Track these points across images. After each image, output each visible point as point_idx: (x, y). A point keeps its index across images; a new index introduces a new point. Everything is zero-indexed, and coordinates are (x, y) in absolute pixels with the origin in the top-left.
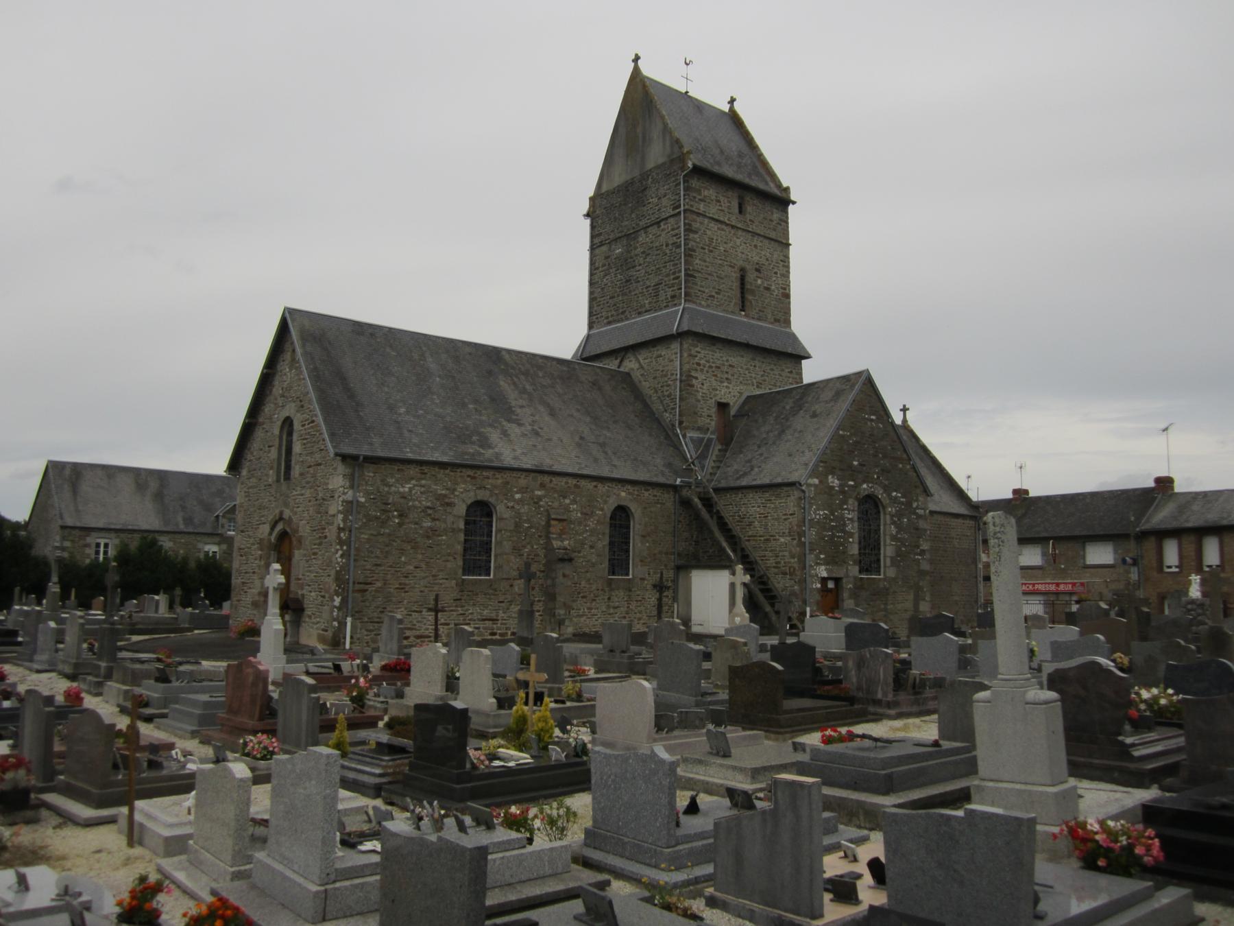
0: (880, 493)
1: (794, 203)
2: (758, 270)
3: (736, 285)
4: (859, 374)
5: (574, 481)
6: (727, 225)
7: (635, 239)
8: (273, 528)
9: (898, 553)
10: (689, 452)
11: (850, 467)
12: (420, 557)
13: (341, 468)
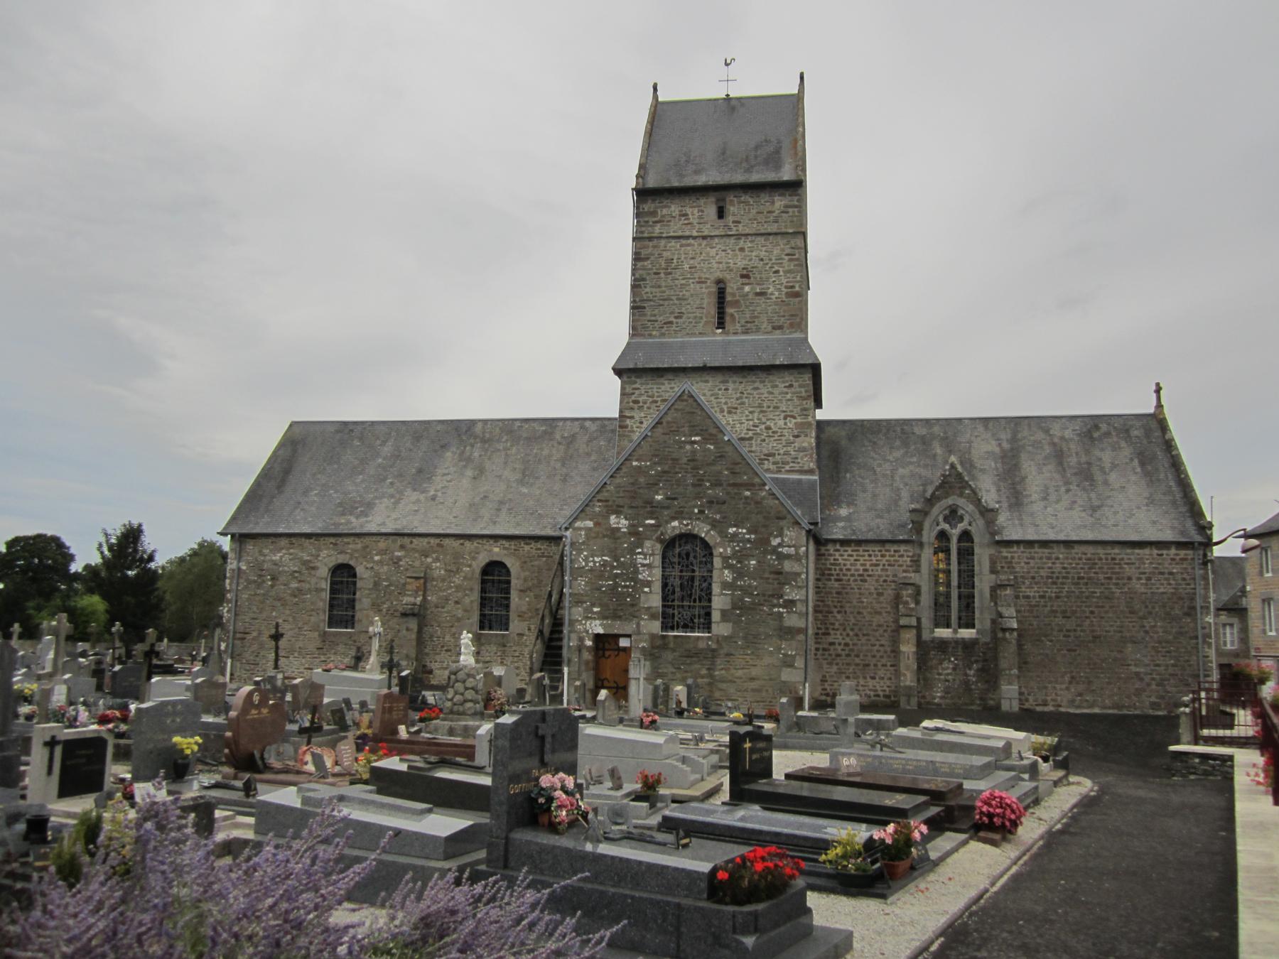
0: (703, 530)
2: (743, 276)
5: (437, 541)
6: (694, 238)
11: (650, 502)
12: (288, 612)
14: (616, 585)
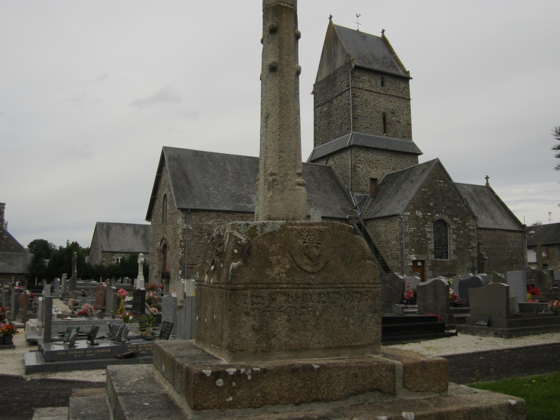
0: (446, 218)
1: (412, 79)
2: (392, 113)
3: (381, 121)
4: (434, 160)
6: (375, 92)
7: (332, 102)
8: (161, 243)
9: (458, 248)
10: (355, 203)
11: (429, 206)
13: (181, 215)
14: (419, 240)
